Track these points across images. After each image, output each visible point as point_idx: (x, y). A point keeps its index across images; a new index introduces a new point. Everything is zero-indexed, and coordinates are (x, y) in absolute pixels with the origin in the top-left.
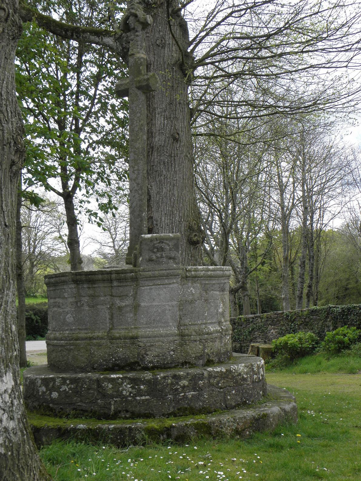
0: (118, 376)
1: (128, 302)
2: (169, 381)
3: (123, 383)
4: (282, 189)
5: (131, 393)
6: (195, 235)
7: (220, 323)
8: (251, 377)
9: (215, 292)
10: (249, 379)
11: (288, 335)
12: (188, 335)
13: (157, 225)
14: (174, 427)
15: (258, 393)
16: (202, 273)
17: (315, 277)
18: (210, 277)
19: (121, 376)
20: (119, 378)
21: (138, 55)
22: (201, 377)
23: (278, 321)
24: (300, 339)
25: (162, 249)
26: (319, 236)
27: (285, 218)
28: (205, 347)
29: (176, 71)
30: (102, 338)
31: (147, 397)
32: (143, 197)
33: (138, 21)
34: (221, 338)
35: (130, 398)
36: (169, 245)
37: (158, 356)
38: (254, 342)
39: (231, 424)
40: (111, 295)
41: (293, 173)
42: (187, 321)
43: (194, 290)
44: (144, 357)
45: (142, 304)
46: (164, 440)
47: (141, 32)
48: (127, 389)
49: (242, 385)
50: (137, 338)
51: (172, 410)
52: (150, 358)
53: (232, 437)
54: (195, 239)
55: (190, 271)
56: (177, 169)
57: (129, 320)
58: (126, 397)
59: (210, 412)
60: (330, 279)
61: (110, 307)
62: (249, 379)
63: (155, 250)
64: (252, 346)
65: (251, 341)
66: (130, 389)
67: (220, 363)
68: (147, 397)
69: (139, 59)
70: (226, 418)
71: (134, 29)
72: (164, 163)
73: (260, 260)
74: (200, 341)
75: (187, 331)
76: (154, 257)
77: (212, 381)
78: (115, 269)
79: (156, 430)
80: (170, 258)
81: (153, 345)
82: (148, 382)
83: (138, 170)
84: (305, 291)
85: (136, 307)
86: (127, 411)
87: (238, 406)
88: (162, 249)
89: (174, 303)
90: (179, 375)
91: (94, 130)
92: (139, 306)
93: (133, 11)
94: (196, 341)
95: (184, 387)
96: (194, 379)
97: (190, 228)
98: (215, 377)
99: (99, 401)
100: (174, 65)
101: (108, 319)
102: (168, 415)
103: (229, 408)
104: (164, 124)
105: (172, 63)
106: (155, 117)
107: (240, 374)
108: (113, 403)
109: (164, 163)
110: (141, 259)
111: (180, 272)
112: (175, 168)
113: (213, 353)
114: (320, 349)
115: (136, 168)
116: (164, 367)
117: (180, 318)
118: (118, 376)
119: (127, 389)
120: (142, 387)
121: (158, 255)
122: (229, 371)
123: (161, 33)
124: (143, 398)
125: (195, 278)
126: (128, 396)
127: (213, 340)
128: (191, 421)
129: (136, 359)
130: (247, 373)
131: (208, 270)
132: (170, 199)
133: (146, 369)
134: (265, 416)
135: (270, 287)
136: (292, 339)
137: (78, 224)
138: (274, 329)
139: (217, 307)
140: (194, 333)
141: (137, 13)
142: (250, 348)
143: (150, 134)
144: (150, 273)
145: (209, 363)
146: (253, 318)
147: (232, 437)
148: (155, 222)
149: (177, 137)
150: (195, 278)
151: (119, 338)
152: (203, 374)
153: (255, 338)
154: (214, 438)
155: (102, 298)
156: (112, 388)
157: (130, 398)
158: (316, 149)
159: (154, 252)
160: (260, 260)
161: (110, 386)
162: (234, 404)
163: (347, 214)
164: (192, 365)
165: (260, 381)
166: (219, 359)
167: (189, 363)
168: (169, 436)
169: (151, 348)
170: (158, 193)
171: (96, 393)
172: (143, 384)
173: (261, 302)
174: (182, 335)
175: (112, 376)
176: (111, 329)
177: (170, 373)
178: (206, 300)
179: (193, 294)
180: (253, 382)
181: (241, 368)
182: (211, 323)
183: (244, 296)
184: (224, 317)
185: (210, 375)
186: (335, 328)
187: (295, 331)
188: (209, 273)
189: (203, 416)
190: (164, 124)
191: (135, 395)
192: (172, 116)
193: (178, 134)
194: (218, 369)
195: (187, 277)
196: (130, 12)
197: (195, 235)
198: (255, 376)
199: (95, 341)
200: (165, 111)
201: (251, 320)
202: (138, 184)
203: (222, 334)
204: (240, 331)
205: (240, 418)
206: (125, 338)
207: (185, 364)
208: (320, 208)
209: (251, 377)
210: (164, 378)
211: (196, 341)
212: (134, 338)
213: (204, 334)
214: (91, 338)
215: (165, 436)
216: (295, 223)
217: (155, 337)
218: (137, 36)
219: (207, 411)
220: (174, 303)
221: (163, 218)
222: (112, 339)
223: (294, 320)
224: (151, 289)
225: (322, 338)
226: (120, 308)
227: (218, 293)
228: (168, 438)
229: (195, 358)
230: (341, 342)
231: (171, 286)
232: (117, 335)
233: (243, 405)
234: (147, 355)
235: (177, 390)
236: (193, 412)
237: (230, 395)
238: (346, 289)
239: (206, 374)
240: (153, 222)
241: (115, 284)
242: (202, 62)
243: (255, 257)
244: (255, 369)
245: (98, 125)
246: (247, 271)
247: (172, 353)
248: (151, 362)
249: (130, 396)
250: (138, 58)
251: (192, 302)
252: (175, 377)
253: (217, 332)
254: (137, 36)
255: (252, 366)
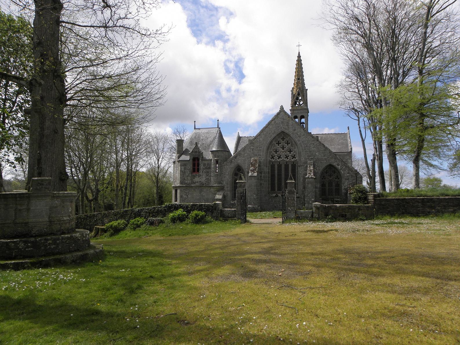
0: (17, 240)
1: (24, 207)
2: (43, 241)
3: (19, 243)
4: (117, 153)
5: (23, 247)
6: (63, 176)
7: (69, 216)
8: (82, 239)
9: (67, 203)
10: (81, 240)
11: (113, 222)
12: (53, 222)
13: (44, 171)
14: (43, 260)
15: (85, 245)
16: (61, 195)
17: (132, 195)
18: (65, 196)
19: (19, 240)
20: (18, 241)
21: (36, 97)
22: (58, 239)
23: (109, 215)
24: (119, 223)
25: (43, 184)
26: (135, 175)
27: (118, 165)
28: (61, 227)
29: (57, 102)
30: (10, 223)
31: (31, 249)
32: (35, 160)
33: (37, 82)
34: (69, 223)
35: (23, 250)
36: (46, 183)
37: (38, 231)
38: (97, 226)
39: (70, 258)
40: (16, 204)
41: (123, 145)
42: (53, 216)
43: (57, 202)
44: (31, 231)
45: (32, 208)
46: (38, 266)
47: (38, 88)
48: (21, 245)
49: (78, 242)
50: (28, 223)
51: (43, 254)
52: (34, 231)
53: (71, 263)
54: (63, 178)
55: (56, 194)
56: (56, 146)
57: (25, 215)
58: (21, 249)
59: (62, 254)
60: (140, 196)
61: (15, 210)
62: (81, 240)
63: (39, 185)
64: (96, 227)
65: (96, 225)
66: (23, 246)
67: (68, 233)
68: (31, 249)
69: (37, 99)
70: (68, 256)
71: (35, 85)
72: (49, 143)
73: (105, 185)
74: (59, 224)
75: (53, 220)
76: (38, 188)
77: (63, 241)
78: (18, 192)
79: (35, 262)
80: (46, 188)
81: (36, 226)
82: (32, 242)
83: (33, 148)
84: (127, 201)
85: (28, 210)
86: (21, 255)
87: (75, 251)
88: (43, 184)
89: (47, 208)
90: (48, 239)
91: (14, 119)
92: (30, 209)
93: (35, 78)
94: (57, 224)
95: (50, 244)
96: (55, 241)
97: (61, 173)
98: (65, 239)
99: (7, 252)
100: (56, 99)
101: (13, 215)
102: (41, 256)
103: (71, 252)
104: (50, 125)
105: (56, 98)
106: (46, 121)
107: (77, 238)
108: (14, 252)
109: (49, 143)
110: (32, 188)
111: (51, 194)
112: (54, 145)
113: (65, 229)
114: (128, 228)
115: (32, 147)
116: (40, 235)
117: (50, 214)
118: (17, 240)
119: (21, 245)
120: (29, 244)
121: (40, 187)
122: (72, 236)
123: (51, 84)
124: (30, 249)
125: (58, 197)
126: (22, 249)
127: (66, 224)
128: (52, 258)
129: (27, 233)
130: (80, 237)
131: (64, 193)
132: (51, 160)
133: (32, 236)
134: (87, 254)
135: (110, 199)
136: (115, 223)
137: (2, 166)
138: (107, 219)
139: (68, 209)
140: (56, 221)
141: (37, 79)
142: (94, 228)
143: (42, 129)
144: (36, 195)
145: (63, 233)
146: (97, 214)
147: (71, 263)
148: (43, 170)
149: (56, 131)
150: (58, 197)
151: (19, 223)
152: (59, 238)
153: (98, 223)
154: (62, 264)
155: (11, 206)
156: (14, 245)
157: (23, 250)
158: (134, 135)
159: (38, 186)
160: (105, 185)
161: (13, 245)
162: (73, 250)
163: (149, 166)
164: (54, 234)
165: (86, 240)
166: (68, 232)
167: (53, 233)
168: (41, 264)
169: (35, 227)
170: (45, 156)
171: (5, 248)
172: (29, 243)
173: (105, 206)
174: (50, 222)
175: (14, 240)
176: (15, 219)
177: (43, 238)
178: (63, 206)
179: (57, 204)
180: (83, 241)
181: (78, 235)
182: (65, 216)
183: (96, 203)
184: (72, 214)
185: (63, 238)
186: (135, 218)
187: (117, 220)
188: (65, 195)
189: (58, 256)
190: (50, 125)
191: (26, 248)
192: (54, 122)
193: (57, 130)
194: (67, 236)
195: (54, 196)
196: (33, 78)
197: (63, 176)
198: (84, 238)
199: (6, 225)
200: (51, 119)
201: (96, 215)
202: (33, 154)
203: (70, 221)
204: (90, 220)
205: (75, 255)
206: (22, 223)
207: (51, 234)
208: (136, 162)
209: (82, 239)
210: (40, 240)
211: (57, 224)
212: (26, 223)
213: (61, 221)
214: (4, 224)
215: (39, 265)
216: (123, 168)
217: (37, 222)
218: (36, 89)
219: (60, 253)
220: (47, 208)
221: (47, 168)
222: (16, 224)
223: (117, 215)
224: (36, 202)
225: (129, 223)
226: (20, 210)
227: (69, 203)
228: (40, 266)
229: (56, 231)
230: (137, 225)
231: (46, 200)
232: (18, 222)
233: (78, 250)
234: (33, 230)
235: (46, 245)
236: (54, 254)
237: (72, 246)
238: (148, 200)
239: (60, 238)
240: (42, 170)
241: (18, 199)
242: (71, 99)
243: (103, 184)
244: (85, 235)
245: (17, 117)
246: (98, 191)
247: (45, 229)
248: (34, 234)
249: (23, 248)
250: (36, 99)
251: (56, 207)
252: (45, 239)
253: (68, 220)
254: (36, 89)
255: (83, 234)
